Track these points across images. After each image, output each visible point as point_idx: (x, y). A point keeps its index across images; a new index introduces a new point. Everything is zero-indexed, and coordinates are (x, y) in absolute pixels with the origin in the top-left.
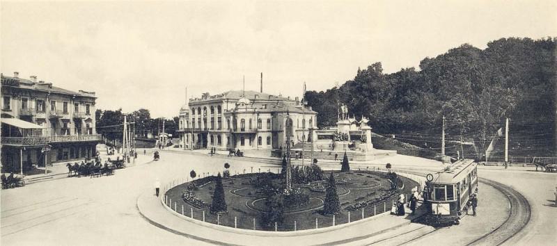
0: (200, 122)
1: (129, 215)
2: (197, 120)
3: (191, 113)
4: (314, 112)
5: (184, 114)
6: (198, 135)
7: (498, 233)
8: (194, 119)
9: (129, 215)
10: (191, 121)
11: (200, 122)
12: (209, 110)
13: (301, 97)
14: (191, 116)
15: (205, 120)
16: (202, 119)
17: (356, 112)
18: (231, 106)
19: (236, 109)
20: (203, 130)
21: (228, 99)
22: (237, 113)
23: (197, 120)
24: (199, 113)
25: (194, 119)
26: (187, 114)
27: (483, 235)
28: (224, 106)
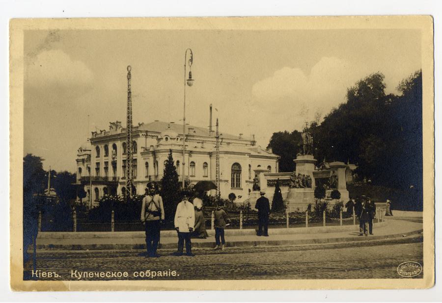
0: (106, 169)
1: (129, 74)
2: (102, 166)
3: (94, 154)
4: (273, 155)
5: (85, 157)
6: (124, 144)
7: (327, 250)
8: (98, 164)
9: (129, 74)
10: (93, 166)
11: (106, 169)
12: (120, 149)
13: (264, 141)
14: (94, 160)
15: (114, 164)
16: (110, 164)
17: (192, 253)
18: (152, 142)
19: (158, 146)
20: (111, 180)
21: (147, 132)
22: (159, 151)
23: (102, 166)
24: (107, 155)
25: (98, 164)
26: (90, 156)
27: (318, 251)
28: (141, 142)
